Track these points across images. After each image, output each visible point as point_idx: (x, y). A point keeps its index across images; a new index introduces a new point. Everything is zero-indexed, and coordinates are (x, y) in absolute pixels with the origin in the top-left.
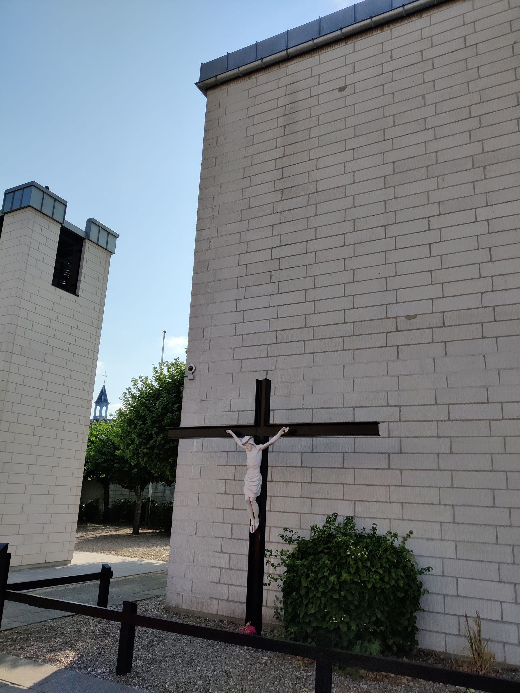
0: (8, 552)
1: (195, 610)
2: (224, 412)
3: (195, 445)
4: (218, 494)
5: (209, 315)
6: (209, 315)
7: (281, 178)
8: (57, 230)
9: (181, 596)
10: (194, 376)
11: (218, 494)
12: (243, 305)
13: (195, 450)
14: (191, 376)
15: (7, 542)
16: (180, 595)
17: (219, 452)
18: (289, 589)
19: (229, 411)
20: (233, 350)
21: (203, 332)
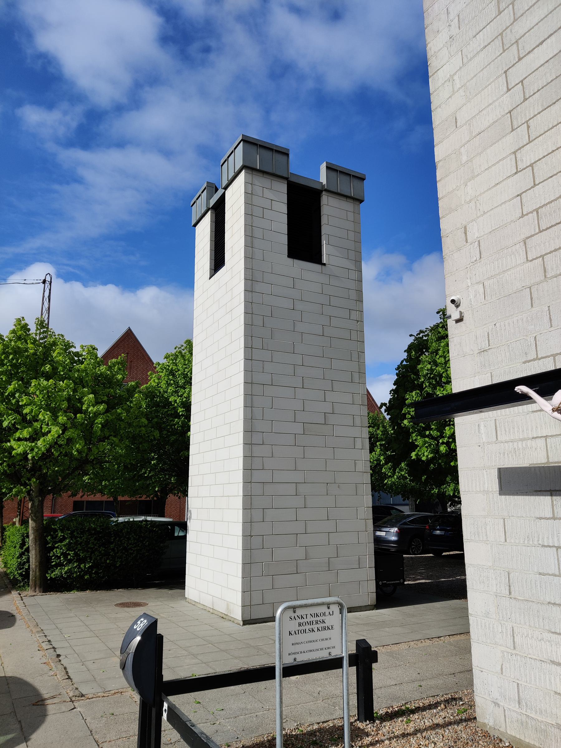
0: (354, 668)
1: (532, 742)
2: (525, 363)
3: (482, 431)
4: (541, 518)
5: (470, 201)
6: (470, 201)
7: (516, 173)
8: (283, 187)
9: (501, 708)
10: (461, 313)
11: (541, 518)
12: (528, 156)
13: (484, 440)
14: (455, 315)
15: (122, 331)
16: (499, 706)
17: (529, 439)
18: (6, 734)
19: (534, 360)
20: (522, 244)
21: (466, 233)
